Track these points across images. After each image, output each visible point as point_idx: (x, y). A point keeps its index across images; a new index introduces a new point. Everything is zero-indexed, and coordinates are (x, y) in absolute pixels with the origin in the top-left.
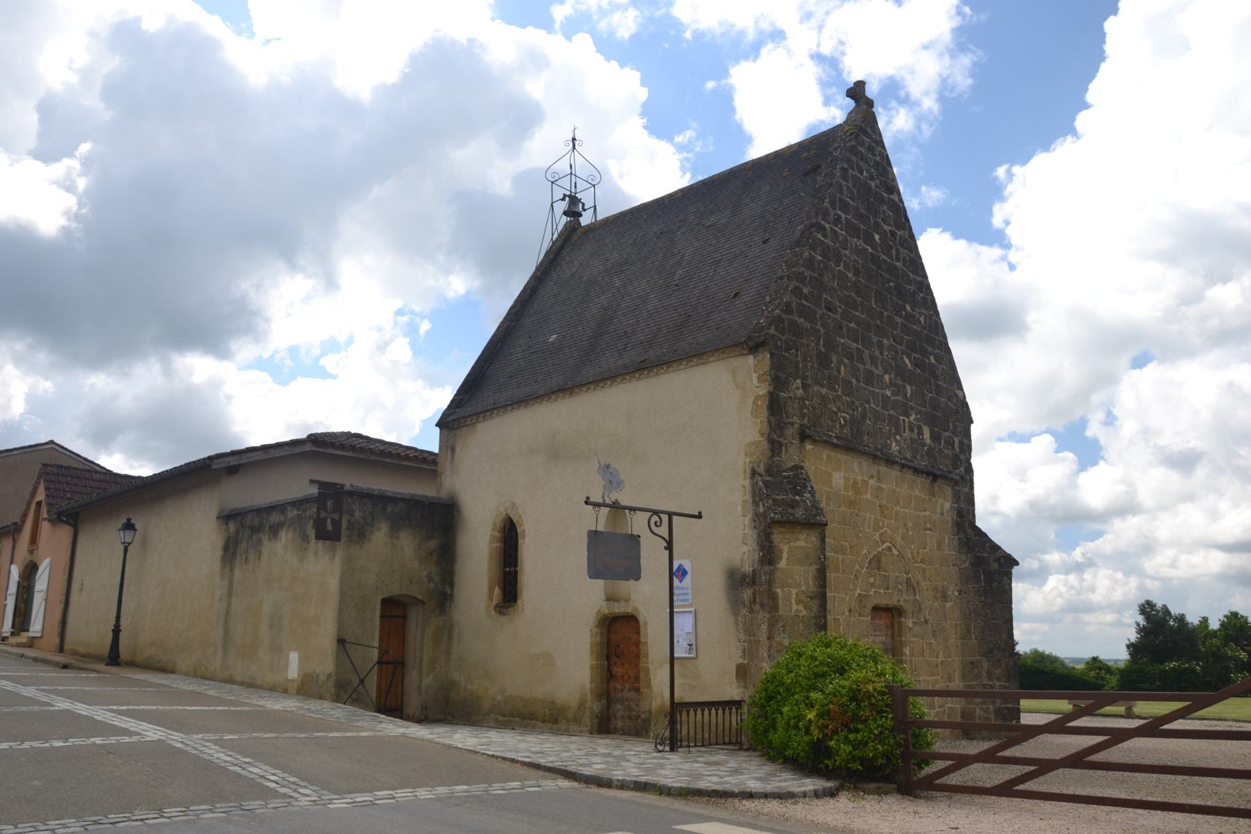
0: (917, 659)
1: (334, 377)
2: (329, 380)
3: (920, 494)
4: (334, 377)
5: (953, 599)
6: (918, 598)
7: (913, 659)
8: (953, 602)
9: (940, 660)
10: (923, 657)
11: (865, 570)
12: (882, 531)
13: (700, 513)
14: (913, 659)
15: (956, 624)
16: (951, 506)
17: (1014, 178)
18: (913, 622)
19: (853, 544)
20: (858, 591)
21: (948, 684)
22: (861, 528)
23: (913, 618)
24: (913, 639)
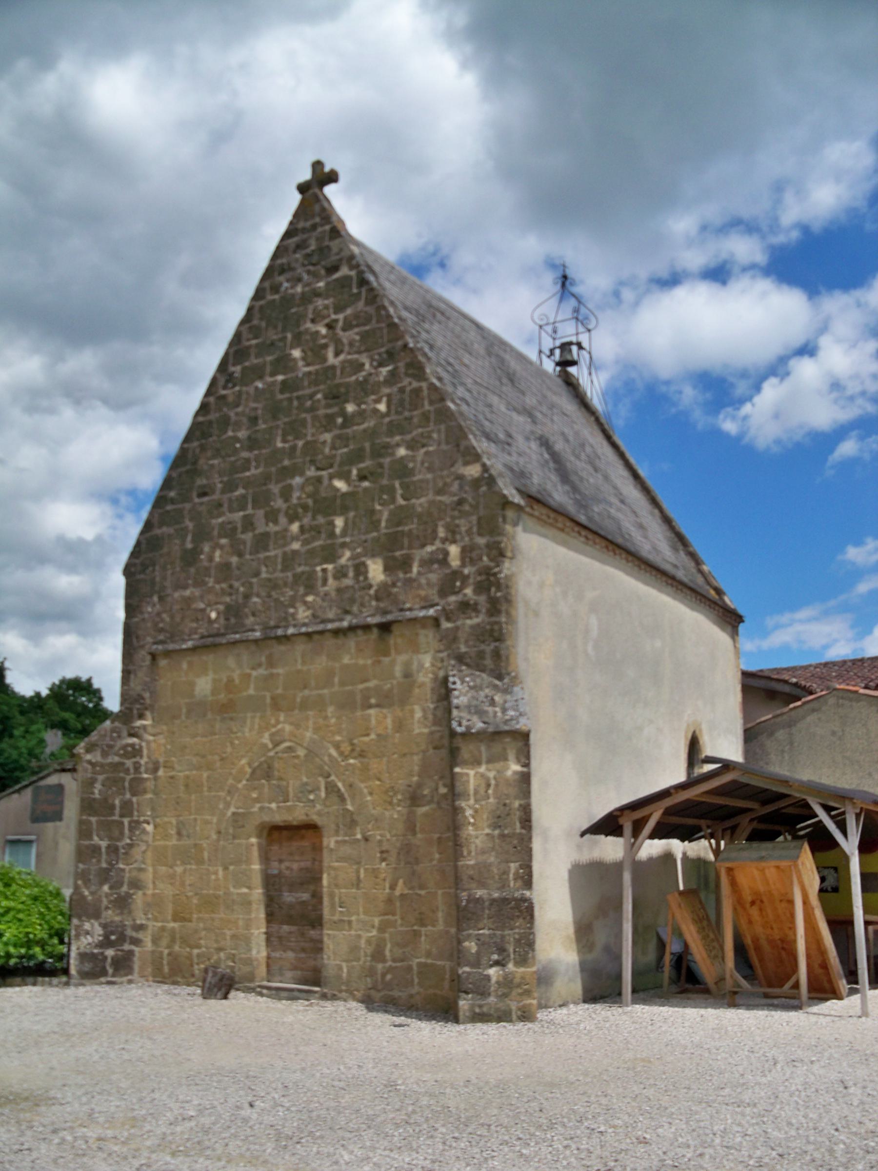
0: (343, 891)
1: (583, 834)
2: (585, 826)
3: (353, 661)
4: (583, 834)
5: (436, 800)
6: (350, 807)
7: (336, 891)
8: (434, 806)
9: (397, 892)
10: (358, 888)
11: (244, 782)
12: (274, 730)
13: (317, 165)
14: (336, 891)
15: (439, 838)
16: (434, 658)
17: (96, 684)
18: (337, 842)
19: (224, 755)
20: (232, 809)
21: (415, 928)
22: (239, 734)
23: (338, 835)
24: (336, 864)
